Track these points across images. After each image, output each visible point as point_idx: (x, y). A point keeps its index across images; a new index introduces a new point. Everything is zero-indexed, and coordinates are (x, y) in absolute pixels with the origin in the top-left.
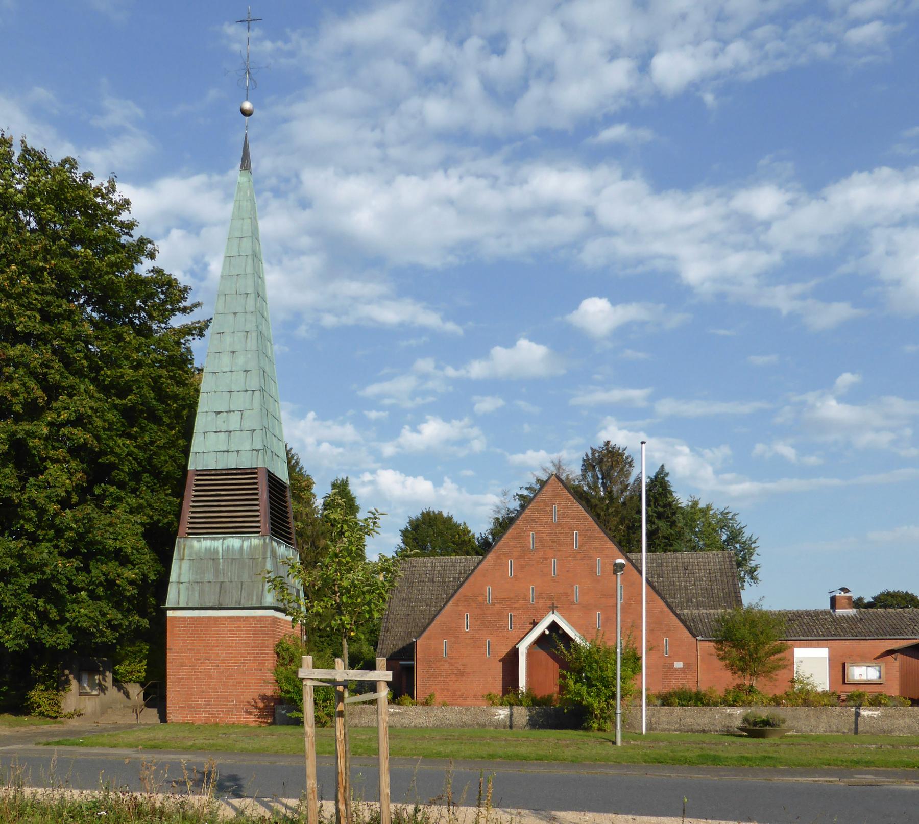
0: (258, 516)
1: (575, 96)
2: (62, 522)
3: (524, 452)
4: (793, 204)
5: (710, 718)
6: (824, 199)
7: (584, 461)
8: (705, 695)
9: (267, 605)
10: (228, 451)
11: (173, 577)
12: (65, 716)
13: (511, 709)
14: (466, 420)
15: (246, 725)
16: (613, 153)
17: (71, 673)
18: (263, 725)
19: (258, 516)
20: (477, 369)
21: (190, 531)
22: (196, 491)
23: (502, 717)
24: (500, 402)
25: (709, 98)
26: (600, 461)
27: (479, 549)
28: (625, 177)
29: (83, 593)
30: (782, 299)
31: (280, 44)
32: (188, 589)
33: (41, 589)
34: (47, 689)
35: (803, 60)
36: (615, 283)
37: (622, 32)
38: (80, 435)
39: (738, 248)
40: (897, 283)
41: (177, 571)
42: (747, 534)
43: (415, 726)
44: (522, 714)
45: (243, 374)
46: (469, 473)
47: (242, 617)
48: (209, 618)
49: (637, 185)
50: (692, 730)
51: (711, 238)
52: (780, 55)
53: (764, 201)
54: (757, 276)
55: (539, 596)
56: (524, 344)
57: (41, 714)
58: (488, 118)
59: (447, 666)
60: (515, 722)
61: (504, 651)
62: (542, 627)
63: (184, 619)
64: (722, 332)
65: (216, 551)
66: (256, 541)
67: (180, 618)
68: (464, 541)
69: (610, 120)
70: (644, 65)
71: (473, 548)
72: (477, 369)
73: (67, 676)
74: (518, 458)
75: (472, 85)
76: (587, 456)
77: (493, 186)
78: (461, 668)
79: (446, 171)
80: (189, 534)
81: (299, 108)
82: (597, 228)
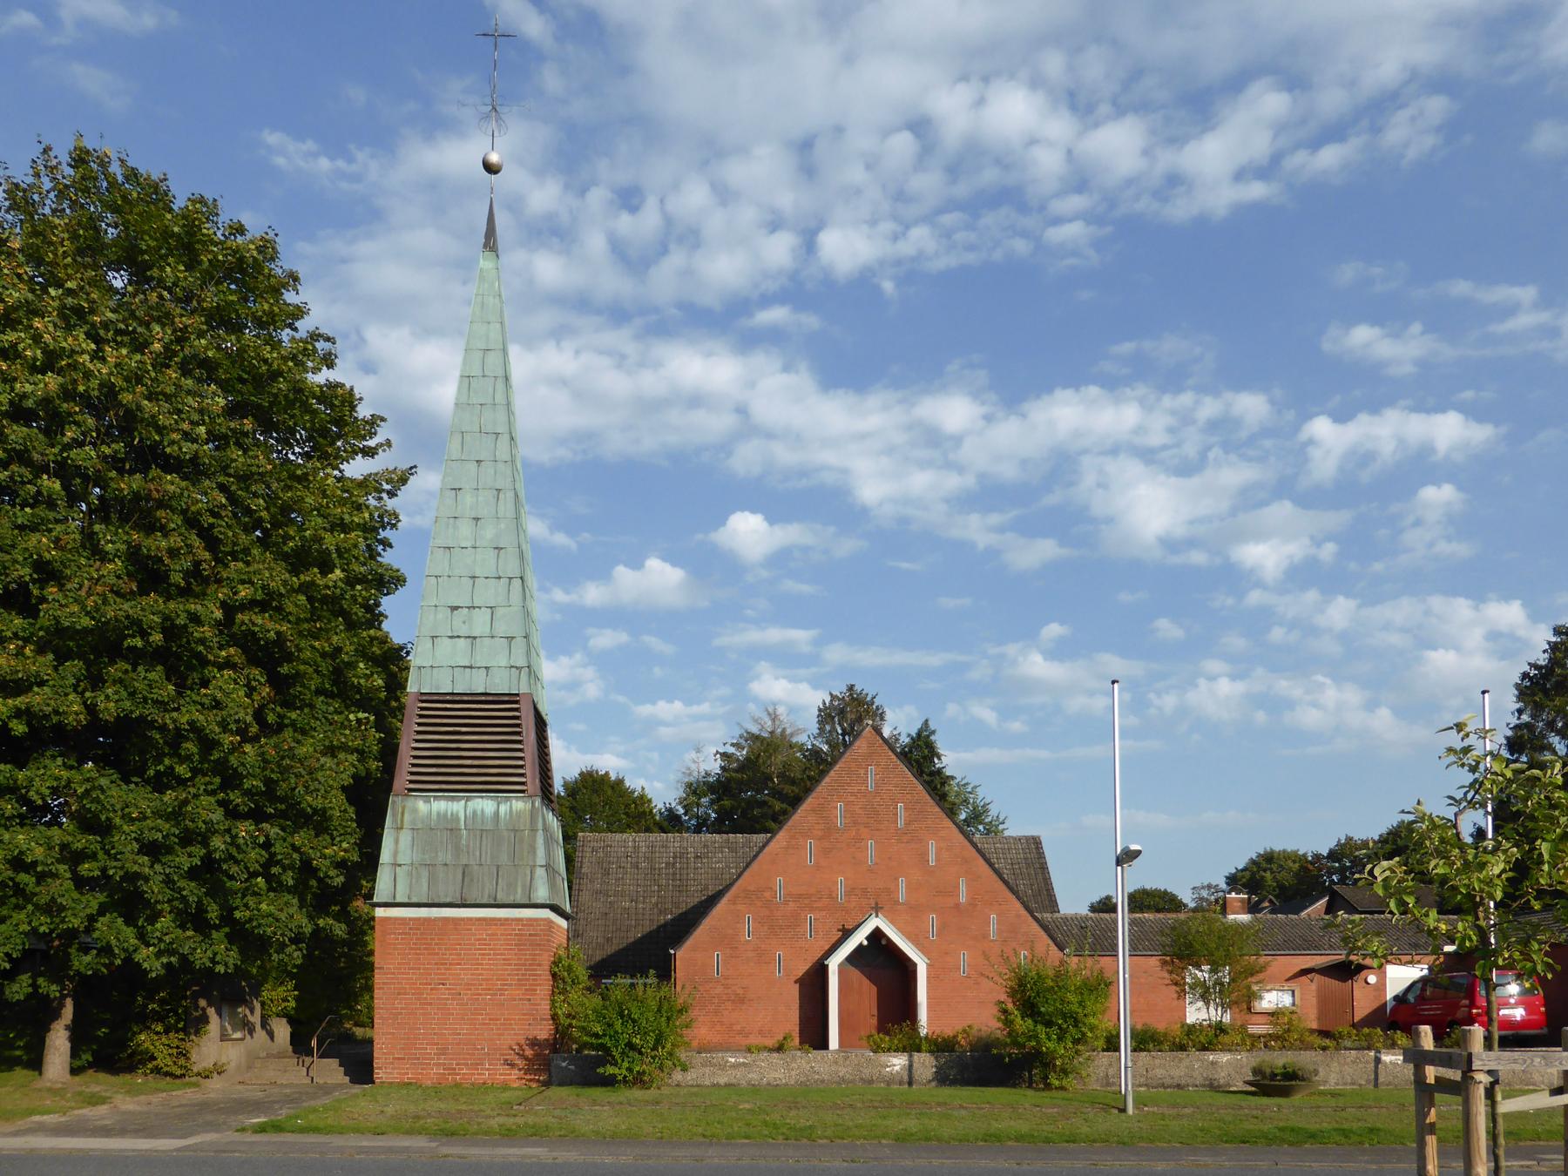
0: (521, 767)
1: (724, 270)
2: (243, 764)
3: (654, 703)
4: (988, 418)
6: (1024, 416)
8: (1165, 1035)
11: (385, 856)
12: (199, 1074)
14: (578, 656)
15: (505, 1087)
16: (772, 338)
17: (210, 1005)
18: (534, 1085)
19: (521, 767)
20: (593, 594)
22: (419, 724)
23: (897, 1068)
24: (623, 637)
25: (888, 286)
26: (842, 712)
27: (665, 824)
28: (787, 368)
30: (976, 529)
31: (341, 163)
32: (410, 874)
33: (208, 871)
34: (167, 1032)
35: (998, 255)
36: (774, 499)
37: (786, 199)
38: (265, 625)
39: (924, 465)
40: (1110, 520)
42: (993, 811)
44: (925, 1064)
45: (493, 553)
46: (581, 727)
48: (446, 920)
49: (803, 379)
50: (1163, 1086)
51: (890, 450)
52: (970, 248)
53: (954, 411)
54: (947, 501)
55: (850, 892)
56: (654, 564)
57: (157, 1070)
58: (612, 283)
60: (916, 1076)
61: (802, 968)
62: (859, 938)
63: (403, 921)
64: (905, 565)
66: (519, 805)
69: (766, 301)
70: (809, 243)
71: (656, 824)
72: (593, 594)
73: (204, 1009)
74: (645, 710)
75: (596, 242)
77: (619, 366)
78: (740, 991)
79: (558, 343)
80: (410, 790)
81: (365, 247)
82: (747, 426)
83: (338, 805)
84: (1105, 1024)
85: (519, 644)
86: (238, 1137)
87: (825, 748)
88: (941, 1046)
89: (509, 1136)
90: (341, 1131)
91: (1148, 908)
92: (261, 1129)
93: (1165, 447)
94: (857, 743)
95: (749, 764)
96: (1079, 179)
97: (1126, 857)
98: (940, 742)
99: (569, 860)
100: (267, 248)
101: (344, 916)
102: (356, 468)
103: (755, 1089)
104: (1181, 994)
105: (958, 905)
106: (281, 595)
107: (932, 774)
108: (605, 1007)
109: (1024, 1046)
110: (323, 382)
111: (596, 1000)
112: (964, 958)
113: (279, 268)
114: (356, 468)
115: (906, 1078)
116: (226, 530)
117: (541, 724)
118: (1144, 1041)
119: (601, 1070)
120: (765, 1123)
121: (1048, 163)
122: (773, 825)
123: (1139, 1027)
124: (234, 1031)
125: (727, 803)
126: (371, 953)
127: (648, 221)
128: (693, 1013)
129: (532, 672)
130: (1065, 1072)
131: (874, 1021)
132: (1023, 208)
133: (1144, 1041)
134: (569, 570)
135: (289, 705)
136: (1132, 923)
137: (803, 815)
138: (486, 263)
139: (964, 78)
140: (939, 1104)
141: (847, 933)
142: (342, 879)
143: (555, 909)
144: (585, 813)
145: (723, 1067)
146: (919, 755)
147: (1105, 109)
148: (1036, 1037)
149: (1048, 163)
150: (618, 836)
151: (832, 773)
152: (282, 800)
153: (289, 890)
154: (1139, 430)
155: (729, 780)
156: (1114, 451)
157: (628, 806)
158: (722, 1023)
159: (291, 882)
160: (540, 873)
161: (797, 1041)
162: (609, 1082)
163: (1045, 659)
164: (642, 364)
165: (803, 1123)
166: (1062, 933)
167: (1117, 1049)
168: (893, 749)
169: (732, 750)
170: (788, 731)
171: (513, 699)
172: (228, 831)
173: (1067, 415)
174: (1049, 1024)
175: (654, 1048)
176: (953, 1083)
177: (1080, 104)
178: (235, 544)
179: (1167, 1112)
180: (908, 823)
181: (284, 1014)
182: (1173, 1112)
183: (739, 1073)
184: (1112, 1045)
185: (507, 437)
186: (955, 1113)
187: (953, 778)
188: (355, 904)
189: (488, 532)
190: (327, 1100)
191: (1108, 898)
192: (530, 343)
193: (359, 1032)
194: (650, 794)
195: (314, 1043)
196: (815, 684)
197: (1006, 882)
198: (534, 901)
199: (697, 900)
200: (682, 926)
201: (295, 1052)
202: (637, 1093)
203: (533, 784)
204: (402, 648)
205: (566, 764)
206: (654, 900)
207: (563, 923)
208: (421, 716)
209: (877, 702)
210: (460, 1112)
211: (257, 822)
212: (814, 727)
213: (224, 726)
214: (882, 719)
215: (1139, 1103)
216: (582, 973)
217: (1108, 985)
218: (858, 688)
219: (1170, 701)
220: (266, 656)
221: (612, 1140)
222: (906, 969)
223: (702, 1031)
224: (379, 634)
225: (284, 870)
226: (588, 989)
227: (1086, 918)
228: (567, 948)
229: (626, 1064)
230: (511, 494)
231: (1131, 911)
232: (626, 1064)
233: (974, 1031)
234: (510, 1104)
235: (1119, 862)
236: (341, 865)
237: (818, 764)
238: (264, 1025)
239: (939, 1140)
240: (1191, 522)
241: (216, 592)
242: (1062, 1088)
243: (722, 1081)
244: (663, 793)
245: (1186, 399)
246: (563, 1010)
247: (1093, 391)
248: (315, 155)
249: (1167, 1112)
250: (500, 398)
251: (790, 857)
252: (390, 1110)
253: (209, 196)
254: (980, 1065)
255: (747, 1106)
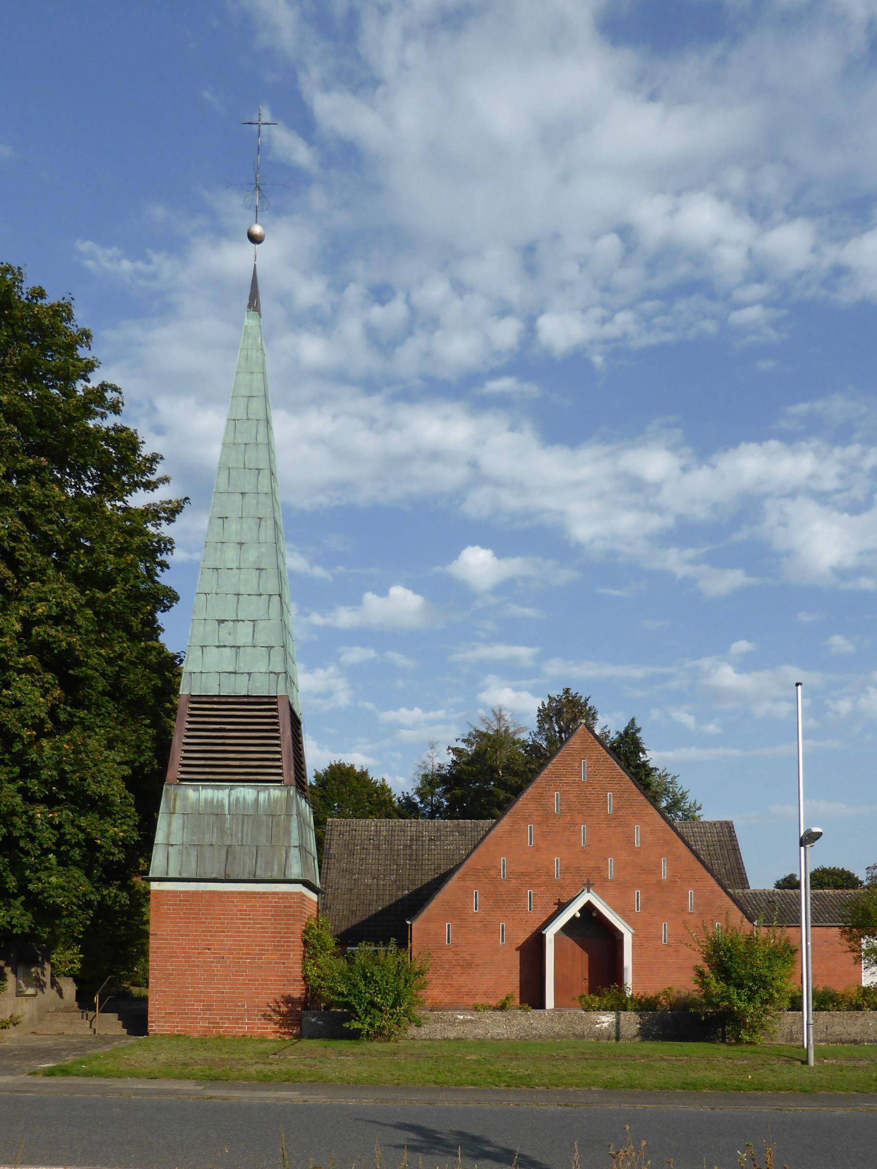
0: (278, 760)
1: (459, 349)
3: (396, 709)
4: (685, 469)
5: (863, 1025)
6: (713, 467)
7: (539, 711)
8: (843, 996)
9: (293, 877)
10: (235, 673)
11: (160, 837)
13: (618, 1014)
14: (331, 669)
15: (262, 1039)
16: (501, 402)
17: (7, 965)
19: (278, 760)
20: (345, 618)
21: (183, 776)
22: (190, 723)
25: (598, 360)
26: (559, 713)
28: (512, 429)
29: (51, 856)
30: (675, 561)
31: (140, 265)
32: (181, 853)
36: (502, 537)
37: (513, 292)
40: (789, 553)
41: (165, 828)
42: (690, 799)
43: (492, 1038)
44: (631, 1021)
47: (258, 893)
50: (841, 1041)
51: (601, 496)
53: (655, 462)
55: (565, 870)
56: (397, 591)
58: (365, 361)
59: (450, 956)
61: (522, 937)
62: (573, 911)
63: (174, 893)
65: (221, 804)
67: (169, 892)
68: (385, 801)
69: (495, 374)
71: (395, 810)
72: (345, 618)
74: (388, 716)
75: (352, 328)
76: (543, 705)
77: (371, 428)
78: (469, 958)
82: (477, 475)
83: (117, 791)
84: (792, 987)
85: (277, 653)
86: (30, 1079)
87: (545, 745)
88: (645, 1006)
89: (266, 1081)
90: (120, 1076)
91: (828, 886)
92: (50, 1073)
93: (838, 491)
94: (572, 740)
95: (478, 757)
96: (758, 270)
97: (809, 839)
98: (644, 737)
99: (319, 842)
100: (62, 312)
101: (126, 887)
102: (138, 500)
103: (480, 1043)
104: (858, 960)
105: (659, 882)
106: (74, 611)
107: (638, 766)
108: (351, 970)
109: (718, 1006)
110: (111, 425)
111: (342, 963)
112: (665, 928)
113: (73, 328)
114: (138, 500)
115: (614, 1034)
116: (25, 552)
117: (296, 723)
118: (824, 1001)
119: (346, 1025)
120: (490, 1073)
121: (731, 258)
122: (498, 812)
123: (820, 989)
124: (27, 986)
125: (458, 792)
126: (148, 922)
127: (397, 310)
128: (427, 977)
129: (289, 678)
130: (752, 1029)
131: (586, 984)
132: (711, 296)
133: (824, 1001)
134: (322, 597)
135: (77, 704)
136: (814, 898)
137: (524, 802)
138: (250, 321)
139: (662, 191)
140: (642, 1057)
141: (562, 907)
142: (122, 856)
143: (307, 884)
144: (334, 801)
145: (452, 1023)
146: (626, 750)
147: (779, 215)
148: (728, 998)
149: (731, 258)
150: (362, 822)
151: (550, 766)
152: (71, 787)
153: (76, 864)
154: (813, 476)
155: (460, 772)
156: (792, 494)
157: (370, 795)
158: (451, 985)
159: (78, 858)
160: (294, 853)
161: (518, 1000)
162: (354, 1035)
163: (736, 672)
164: (389, 425)
165: (522, 1072)
166: (752, 906)
167: (800, 1009)
168: (603, 745)
169: (462, 746)
170: (512, 730)
171: (271, 700)
172: (26, 812)
173: (752, 465)
174: (740, 986)
175: (393, 1007)
176: (656, 1038)
177: (758, 211)
178: (34, 565)
179: (845, 1064)
180: (616, 810)
181: (70, 974)
182: (851, 1064)
183: (466, 1029)
184: (796, 1005)
185: (268, 472)
186: (657, 1064)
187: (656, 769)
188: (135, 879)
189: (251, 555)
190: (107, 1049)
191: (792, 876)
192: (295, 408)
193: (135, 991)
194: (389, 783)
195: (96, 999)
196: (535, 693)
197: (702, 862)
198: (289, 877)
199: (430, 878)
200: (418, 900)
201: (80, 1007)
202: (377, 1046)
203: (288, 774)
204: (176, 657)
205: (317, 759)
206: (393, 878)
207: (314, 897)
208: (191, 716)
209: (590, 704)
210: (222, 1060)
211: (50, 806)
212: (534, 726)
213: (21, 719)
214: (594, 719)
215: (820, 1056)
216: (330, 941)
217: (793, 952)
218: (573, 692)
219: (845, 706)
220: (60, 664)
221: (355, 1085)
222: (614, 938)
223: (434, 992)
224: (156, 644)
225: (72, 847)
226: (334, 954)
227: (773, 893)
228: (317, 919)
229: (368, 1020)
230: (270, 523)
231: (812, 887)
232: (368, 1020)
233: (674, 993)
234: (266, 1053)
235: (802, 843)
236: (125, 845)
237: (538, 758)
238: (54, 983)
239: (642, 1088)
240: (860, 554)
241: (17, 609)
242: (750, 1043)
243: (452, 1035)
244: (402, 783)
245: (853, 450)
246: (313, 972)
247: (773, 444)
248: (119, 259)
249: (845, 1064)
250: (261, 438)
251: (513, 840)
252: (162, 1058)
253: (15, 264)
254: (679, 1022)
255: (474, 1057)
